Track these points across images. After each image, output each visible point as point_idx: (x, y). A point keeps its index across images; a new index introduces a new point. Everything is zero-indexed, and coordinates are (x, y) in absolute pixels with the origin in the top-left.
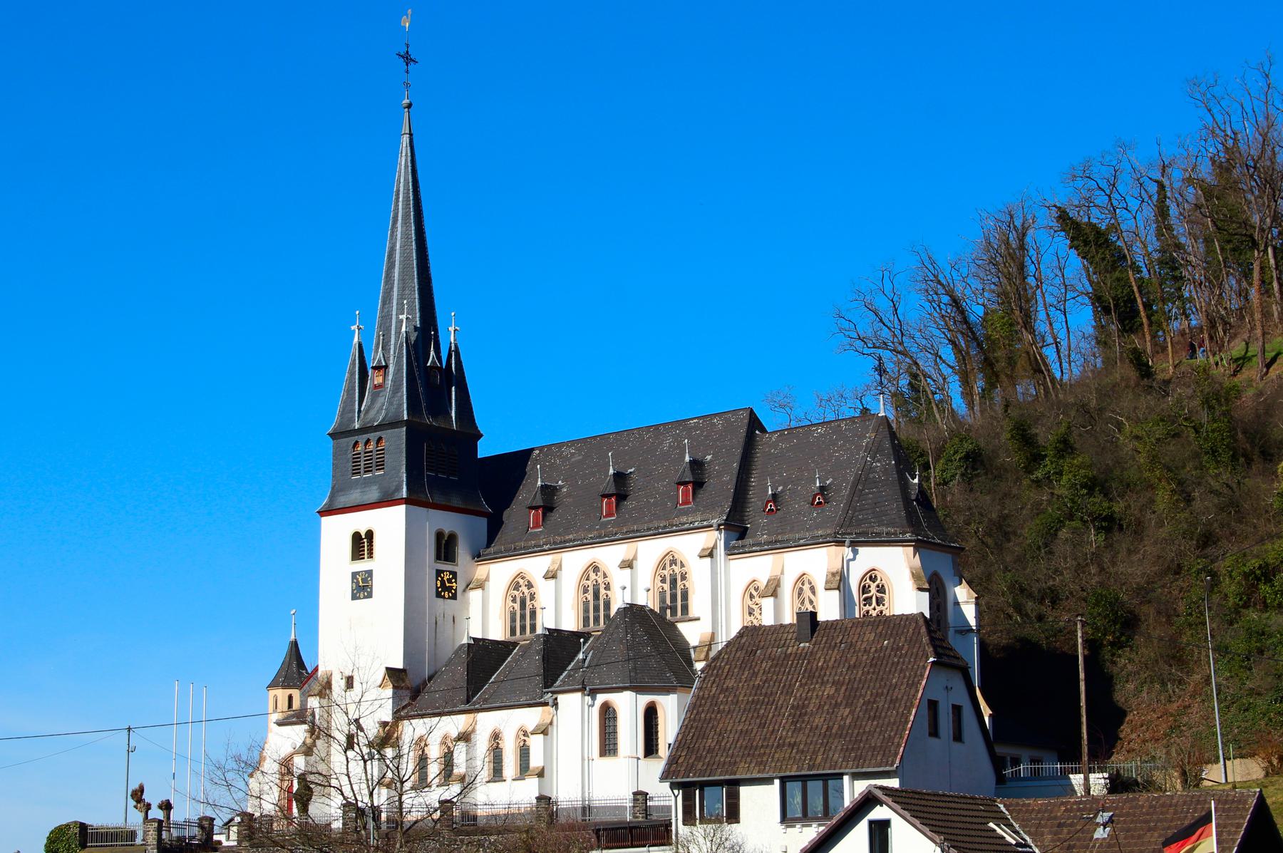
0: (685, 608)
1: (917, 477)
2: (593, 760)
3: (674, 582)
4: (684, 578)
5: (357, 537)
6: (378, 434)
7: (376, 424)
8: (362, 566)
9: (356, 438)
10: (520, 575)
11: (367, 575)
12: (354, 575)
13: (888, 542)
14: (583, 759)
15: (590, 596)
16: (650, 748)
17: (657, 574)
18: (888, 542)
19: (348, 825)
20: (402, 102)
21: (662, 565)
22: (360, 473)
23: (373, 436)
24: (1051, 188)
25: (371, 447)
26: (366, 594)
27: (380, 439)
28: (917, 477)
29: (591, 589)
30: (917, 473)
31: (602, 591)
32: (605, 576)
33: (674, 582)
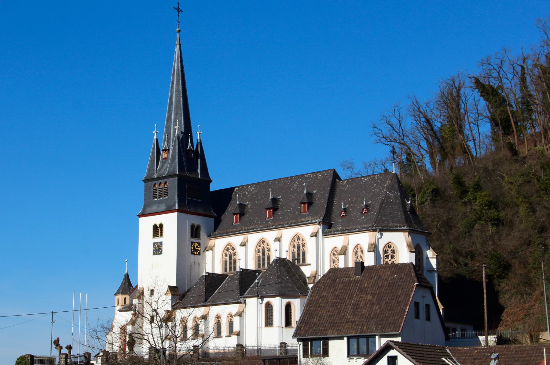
0: (304, 260)
3: (299, 248)
5: (155, 227)
6: (165, 180)
7: (164, 176)
10: (229, 244)
15: (261, 254)
23: (163, 181)
30: (410, 199)
31: (266, 252)
32: (268, 245)
33: (299, 248)
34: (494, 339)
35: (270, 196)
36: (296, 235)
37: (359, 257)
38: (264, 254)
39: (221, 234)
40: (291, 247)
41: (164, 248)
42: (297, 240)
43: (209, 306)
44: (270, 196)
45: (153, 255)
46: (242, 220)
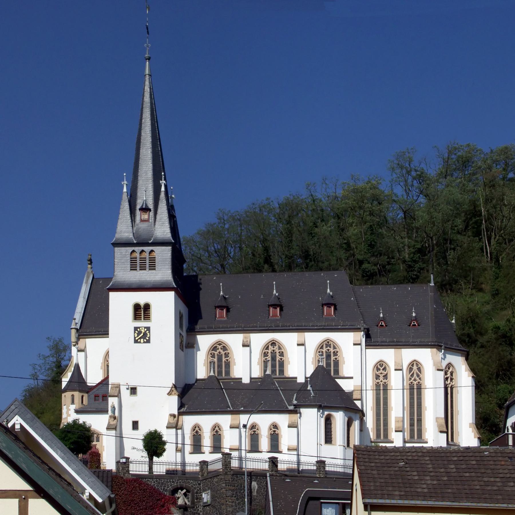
0: (337, 371)
1: (454, 319)
2: (321, 445)
3: (328, 356)
4: (335, 354)
5: (137, 307)
6: (151, 248)
7: (150, 242)
8: (142, 324)
9: (133, 248)
10: (273, 343)
11: (146, 330)
12: (136, 329)
13: (450, 348)
14: (318, 444)
15: (269, 358)
16: (508, 427)
17: (210, 353)
18: (450, 348)
19: (228, 465)
20: (145, 55)
21: (214, 348)
22: (136, 269)
23: (147, 249)
24: (385, 181)
25: (144, 255)
26: (145, 340)
27: (152, 251)
28: (454, 319)
29: (269, 355)
30: (454, 318)
31: (278, 358)
32: (280, 348)
33: (328, 356)
34: (266, 468)
35: (222, 292)
36: (326, 340)
37: (415, 375)
38: (274, 359)
39: (228, 328)
40: (209, 356)
41: (153, 335)
42: (326, 347)
43: (239, 414)
44: (222, 292)
45: (135, 343)
46: (229, 316)
